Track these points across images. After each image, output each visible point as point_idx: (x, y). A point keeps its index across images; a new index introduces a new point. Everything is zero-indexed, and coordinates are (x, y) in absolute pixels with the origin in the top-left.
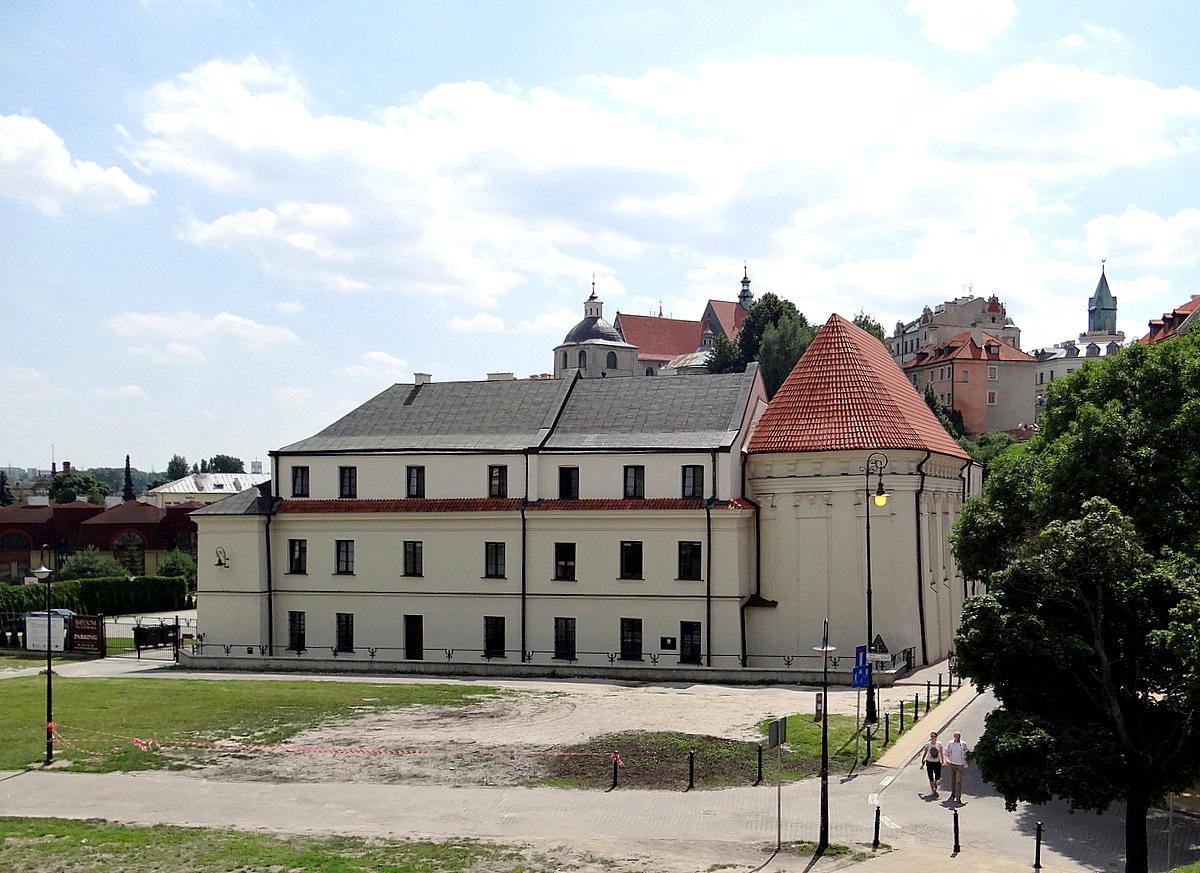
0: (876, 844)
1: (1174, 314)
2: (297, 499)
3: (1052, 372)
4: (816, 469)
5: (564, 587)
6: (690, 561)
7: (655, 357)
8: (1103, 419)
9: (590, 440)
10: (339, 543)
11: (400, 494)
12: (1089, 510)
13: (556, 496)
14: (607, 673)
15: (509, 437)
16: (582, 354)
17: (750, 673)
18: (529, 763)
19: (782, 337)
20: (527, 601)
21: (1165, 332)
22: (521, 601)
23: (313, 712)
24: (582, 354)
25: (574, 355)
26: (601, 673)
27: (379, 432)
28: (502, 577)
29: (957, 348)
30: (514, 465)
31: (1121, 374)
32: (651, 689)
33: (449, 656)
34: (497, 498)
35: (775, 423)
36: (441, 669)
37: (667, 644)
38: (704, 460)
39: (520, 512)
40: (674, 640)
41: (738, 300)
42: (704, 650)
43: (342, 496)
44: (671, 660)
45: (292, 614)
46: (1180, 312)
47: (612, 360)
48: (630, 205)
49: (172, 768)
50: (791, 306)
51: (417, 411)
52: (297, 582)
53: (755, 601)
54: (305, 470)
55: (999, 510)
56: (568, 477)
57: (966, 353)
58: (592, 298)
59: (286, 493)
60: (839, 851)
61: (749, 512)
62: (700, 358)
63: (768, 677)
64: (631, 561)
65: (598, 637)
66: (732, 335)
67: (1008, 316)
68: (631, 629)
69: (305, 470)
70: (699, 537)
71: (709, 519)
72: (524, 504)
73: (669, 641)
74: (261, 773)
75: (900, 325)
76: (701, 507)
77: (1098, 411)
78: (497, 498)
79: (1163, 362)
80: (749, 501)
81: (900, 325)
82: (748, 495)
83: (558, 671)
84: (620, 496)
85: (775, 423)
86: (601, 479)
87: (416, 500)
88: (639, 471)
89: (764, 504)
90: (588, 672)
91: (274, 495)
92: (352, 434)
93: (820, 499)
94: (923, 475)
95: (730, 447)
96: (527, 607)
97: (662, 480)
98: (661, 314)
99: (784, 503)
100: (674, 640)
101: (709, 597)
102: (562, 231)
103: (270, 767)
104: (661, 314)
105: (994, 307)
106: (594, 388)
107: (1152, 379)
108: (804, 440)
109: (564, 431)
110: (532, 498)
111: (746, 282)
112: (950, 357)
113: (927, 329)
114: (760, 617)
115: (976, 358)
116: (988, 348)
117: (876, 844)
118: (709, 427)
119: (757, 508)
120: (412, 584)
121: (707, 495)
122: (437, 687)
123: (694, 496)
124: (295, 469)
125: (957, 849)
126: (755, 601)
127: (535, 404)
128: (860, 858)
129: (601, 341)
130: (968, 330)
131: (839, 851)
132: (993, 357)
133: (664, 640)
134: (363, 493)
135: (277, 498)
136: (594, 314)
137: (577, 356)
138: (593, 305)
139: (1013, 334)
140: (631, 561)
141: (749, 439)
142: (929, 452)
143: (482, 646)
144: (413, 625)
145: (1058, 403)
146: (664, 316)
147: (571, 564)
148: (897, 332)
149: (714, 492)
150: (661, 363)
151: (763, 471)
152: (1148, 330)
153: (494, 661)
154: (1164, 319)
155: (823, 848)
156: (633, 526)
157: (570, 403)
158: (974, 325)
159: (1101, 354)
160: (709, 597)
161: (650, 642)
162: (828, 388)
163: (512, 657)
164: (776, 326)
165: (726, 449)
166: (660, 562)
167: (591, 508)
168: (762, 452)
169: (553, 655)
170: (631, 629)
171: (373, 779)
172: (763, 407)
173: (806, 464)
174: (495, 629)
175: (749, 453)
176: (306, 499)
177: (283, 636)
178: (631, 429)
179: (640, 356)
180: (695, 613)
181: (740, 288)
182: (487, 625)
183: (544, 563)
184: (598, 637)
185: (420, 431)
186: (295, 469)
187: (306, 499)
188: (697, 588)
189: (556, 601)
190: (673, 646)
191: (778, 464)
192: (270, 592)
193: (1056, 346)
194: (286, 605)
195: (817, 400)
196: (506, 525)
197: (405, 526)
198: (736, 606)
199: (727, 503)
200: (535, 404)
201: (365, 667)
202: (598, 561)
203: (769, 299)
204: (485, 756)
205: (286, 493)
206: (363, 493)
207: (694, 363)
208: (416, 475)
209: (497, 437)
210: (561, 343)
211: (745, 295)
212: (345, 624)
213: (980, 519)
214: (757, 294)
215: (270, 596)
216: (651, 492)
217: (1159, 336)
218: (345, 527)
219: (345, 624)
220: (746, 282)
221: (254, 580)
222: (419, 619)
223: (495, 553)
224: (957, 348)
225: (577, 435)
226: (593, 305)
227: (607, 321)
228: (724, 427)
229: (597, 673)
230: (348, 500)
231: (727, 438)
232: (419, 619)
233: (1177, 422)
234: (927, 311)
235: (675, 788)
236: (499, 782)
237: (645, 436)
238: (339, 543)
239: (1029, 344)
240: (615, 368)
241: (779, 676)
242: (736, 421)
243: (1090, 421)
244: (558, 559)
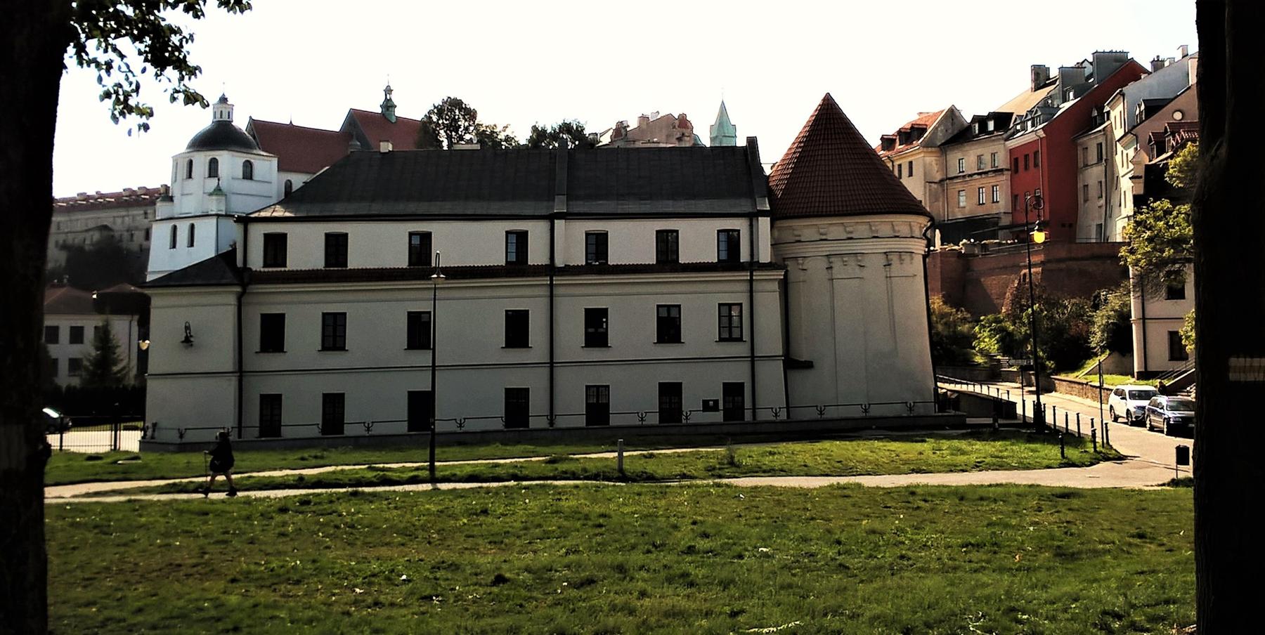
1: (912, 128)
2: (266, 270)
5: (596, 354)
11: (402, 261)
34: (517, 266)
37: (708, 406)
40: (716, 402)
45: (263, 397)
52: (273, 361)
54: (282, 238)
59: (256, 261)
64: (669, 327)
68: (671, 392)
72: (550, 270)
73: (711, 403)
91: (239, 263)
100: (716, 402)
101: (552, 364)
110: (559, 263)
121: (744, 257)
124: (268, 237)
126: (793, 364)
133: (705, 403)
134: (355, 261)
135: (246, 268)
140: (669, 327)
143: (319, 421)
147: (591, 330)
149: (752, 255)
156: (670, 291)
160: (753, 358)
161: (690, 403)
170: (671, 392)
174: (517, 400)
176: (283, 269)
180: (738, 373)
183: (573, 330)
187: (283, 269)
188: (423, 358)
190: (715, 408)
192: (241, 371)
205: (256, 261)
206: (355, 261)
216: (686, 256)
218: (334, 299)
219: (333, 405)
221: (224, 359)
223: (517, 330)
244: (587, 325)
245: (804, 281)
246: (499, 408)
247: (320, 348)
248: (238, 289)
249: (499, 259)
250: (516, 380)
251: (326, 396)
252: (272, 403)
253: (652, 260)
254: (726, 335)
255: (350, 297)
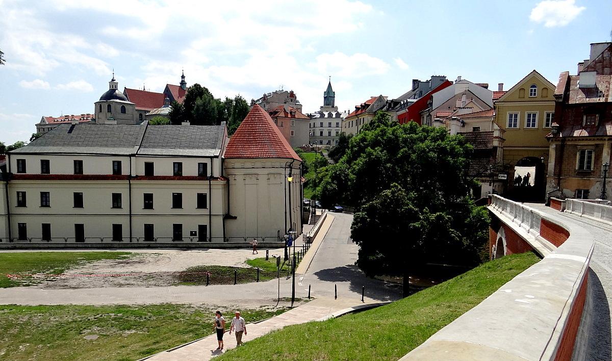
0: (309, 297)
1: (365, 104)
3: (314, 123)
4: (252, 165)
5: (148, 212)
6: (202, 201)
7: (143, 109)
8: (374, 153)
9: (157, 151)
10: (42, 193)
12: (392, 187)
13: (143, 174)
14: (172, 246)
15: (120, 149)
16: (109, 106)
17: (228, 244)
18: (170, 278)
19: (204, 103)
20: (212, 218)
21: (362, 111)
22: (129, 218)
23: (73, 262)
24: (109, 106)
25: (105, 106)
26: (170, 245)
27: (58, 145)
28: (49, 206)
29: (278, 112)
30: (125, 162)
31: (379, 138)
32: (193, 251)
33: (102, 241)
35: (235, 147)
36: (98, 246)
38: (208, 161)
39: (128, 181)
40: (196, 232)
41: (179, 85)
42: (208, 236)
43: (42, 172)
44: (196, 240)
46: (368, 103)
47: (123, 110)
48: (111, 31)
49: (24, 286)
50: (207, 90)
51: (75, 136)
52: (22, 210)
53: (228, 217)
54: (24, 161)
55: (335, 184)
56: (149, 167)
57: (282, 115)
58: (113, 80)
59: (14, 171)
60: (299, 300)
61: (225, 182)
62: (166, 110)
63: (237, 245)
64: (177, 201)
65: (163, 230)
66: (181, 101)
67: (297, 99)
68: (178, 228)
69: (48, 162)
70: (205, 191)
71: (210, 184)
72: (129, 177)
74: (63, 286)
75: (253, 101)
76: (207, 180)
77: (373, 151)
78: (117, 174)
79: (393, 134)
80: (226, 178)
81: (253, 101)
82: (224, 175)
83: (151, 245)
84: (172, 175)
85: (235, 147)
86: (163, 168)
87: (79, 173)
88: (180, 164)
89: (231, 178)
90: (165, 245)
91: (8, 171)
92: (44, 146)
93: (254, 178)
94: (292, 168)
95: (218, 156)
96: (212, 221)
97: (191, 168)
98: (144, 89)
99: (240, 179)
100: (196, 232)
102: (77, 41)
103: (66, 284)
104: (144, 89)
105: (292, 95)
106: (157, 129)
107: (390, 139)
108: (248, 154)
109: (145, 147)
110: (133, 175)
111: (183, 77)
112: (276, 116)
113: (265, 103)
114: (230, 223)
115: (286, 116)
116: (291, 113)
117: (309, 297)
118: (208, 147)
119: (228, 180)
120: (78, 211)
121: (209, 175)
122: (102, 253)
123: (203, 175)
124: (18, 160)
125: (336, 297)
127: (130, 135)
128: (307, 301)
129: (118, 101)
130: (282, 104)
131: (299, 300)
132: (293, 116)
133: (191, 232)
134: (53, 171)
135: (10, 173)
136: (114, 88)
137: (107, 106)
138: (113, 85)
139: (299, 107)
140: (177, 201)
141: (224, 153)
142: (294, 159)
144: (79, 229)
145: (355, 147)
146: (146, 90)
148: (252, 104)
149: (212, 173)
150: (146, 112)
151: (230, 166)
152: (355, 109)
153: (176, 242)
154: (361, 105)
155: (293, 299)
156: (178, 187)
157: (146, 135)
158: (285, 103)
159: (325, 117)
160: (130, 215)
161: (185, 233)
162: (256, 134)
163: (126, 240)
164: (201, 98)
165: (217, 157)
166: (33, 199)
167: (158, 180)
168: (230, 158)
169: (112, 239)
170: (178, 228)
171: (111, 286)
172: (228, 140)
173: (248, 163)
174: (117, 229)
175: (225, 158)
177: (16, 233)
178: (175, 147)
179: (137, 108)
180: (205, 221)
181: (180, 80)
182: (43, 227)
183: (139, 202)
184: (163, 230)
185: (78, 145)
186: (18, 160)
188: (205, 212)
189: (147, 218)
191: (237, 163)
192: (9, 215)
193: (316, 112)
194: (17, 220)
195: (252, 138)
196: (123, 186)
197: (41, 186)
198: (221, 219)
199: (218, 178)
200: (130, 135)
201: (63, 246)
202: (162, 200)
203: (197, 86)
204: (150, 276)
205: (14, 171)
206: (53, 171)
207: (162, 112)
208: (78, 165)
209: (115, 149)
210: (98, 100)
211: (183, 83)
212: (46, 228)
213: (329, 187)
214: (190, 84)
215: (131, 217)
216: (185, 173)
217: (359, 112)
219: (46, 228)
220: (183, 77)
222: (82, 225)
223: (117, 199)
224: (278, 112)
225: (151, 149)
226: (113, 85)
227: (120, 91)
228: (214, 148)
229: (167, 245)
230: (45, 173)
231: (216, 152)
232: (49, 225)
233: (399, 155)
234: (265, 95)
235: (230, 284)
236: (163, 285)
237: (181, 150)
238: (42, 193)
239: (305, 111)
240: (125, 113)
241: (242, 245)
242: (219, 145)
243: (370, 154)
245: (235, 184)
246: (72, 233)
247: (172, 207)
248: (5, 182)
249: (71, 171)
250: (118, 221)
251: (174, 225)
252: (23, 228)
253: (111, 173)
254: (44, 203)
255: (84, 186)
